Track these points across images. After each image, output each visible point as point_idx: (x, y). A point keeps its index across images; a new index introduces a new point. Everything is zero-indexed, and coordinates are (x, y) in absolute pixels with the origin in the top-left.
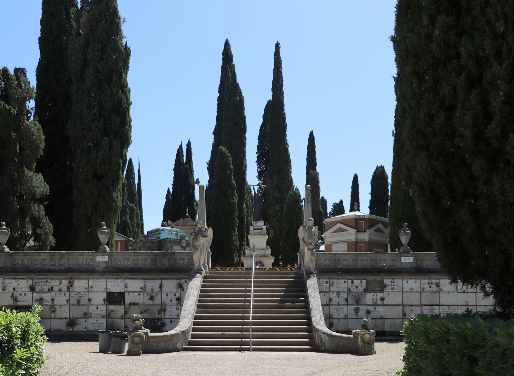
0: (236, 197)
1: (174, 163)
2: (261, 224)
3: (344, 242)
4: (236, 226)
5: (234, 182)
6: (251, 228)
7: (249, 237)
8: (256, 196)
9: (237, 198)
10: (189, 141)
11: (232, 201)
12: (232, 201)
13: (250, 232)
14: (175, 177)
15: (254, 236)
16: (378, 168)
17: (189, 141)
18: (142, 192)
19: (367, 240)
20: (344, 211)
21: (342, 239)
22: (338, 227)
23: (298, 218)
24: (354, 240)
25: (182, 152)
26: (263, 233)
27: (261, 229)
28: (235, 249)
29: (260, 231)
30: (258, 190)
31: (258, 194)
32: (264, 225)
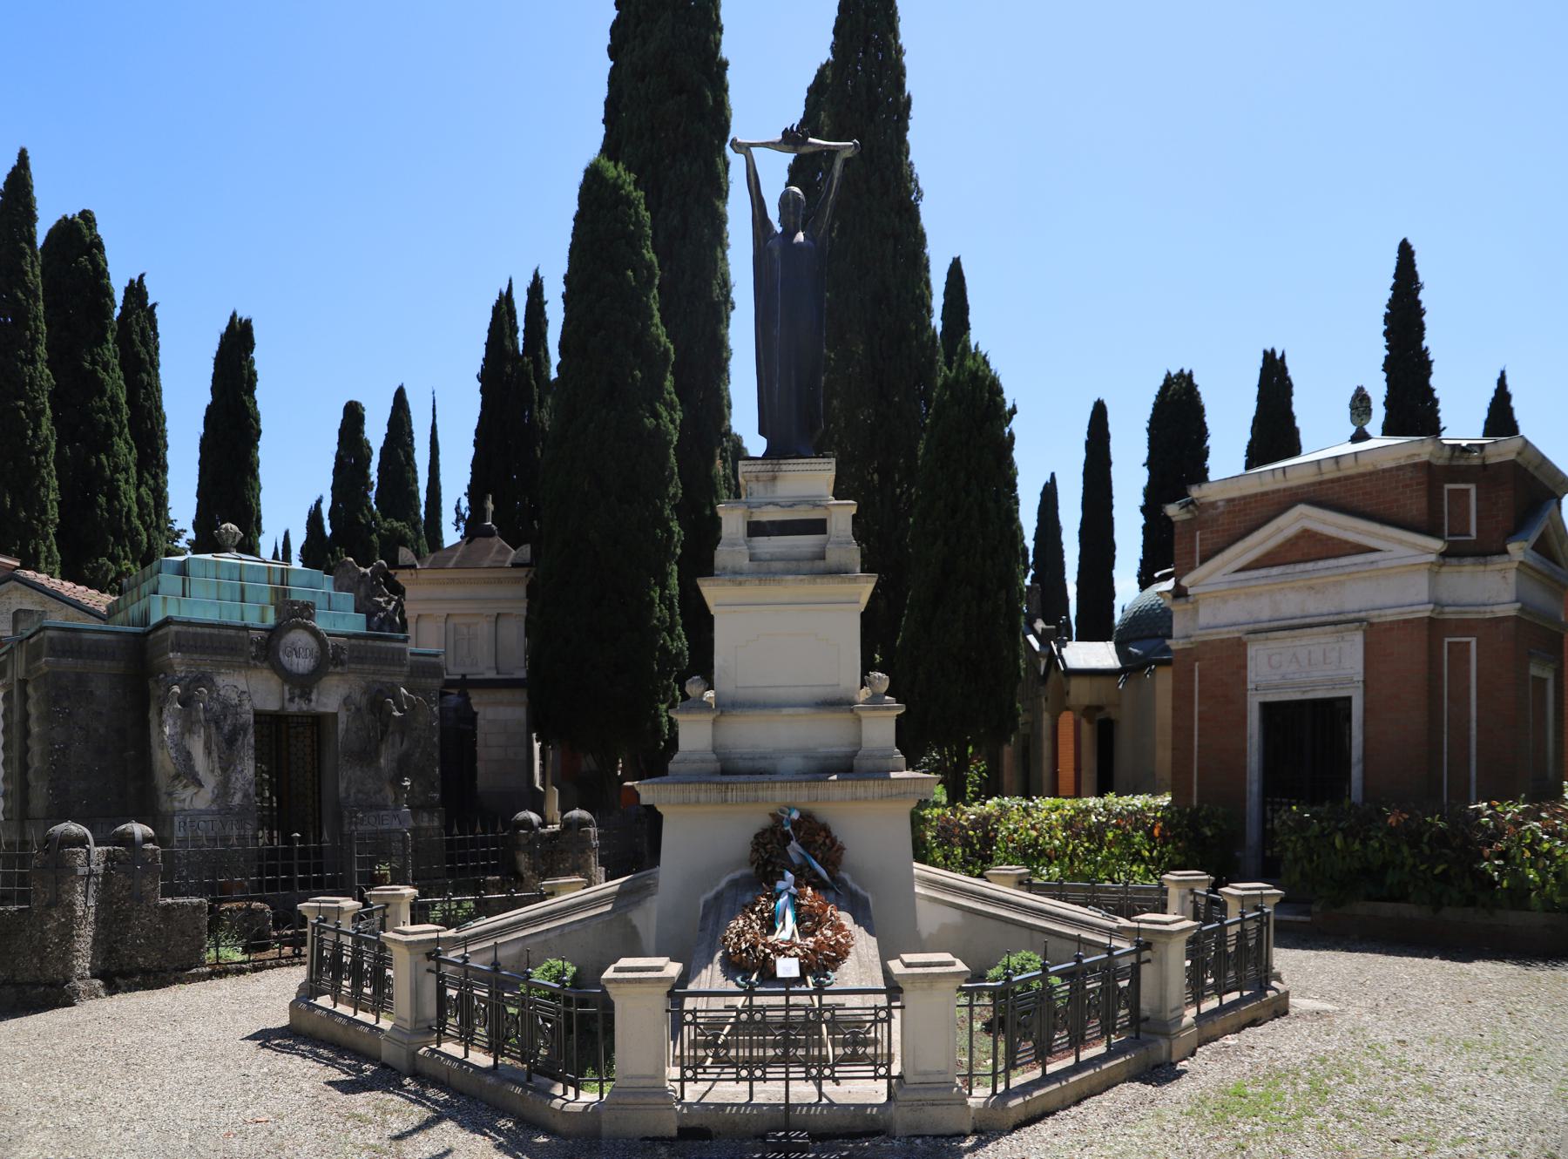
0: (670, 407)
1: (483, 353)
3: (1337, 623)
5: (661, 332)
6: (732, 520)
7: (712, 592)
8: (776, 248)
9: (678, 416)
10: (536, 276)
11: (650, 422)
12: (650, 422)
13: (722, 556)
14: (485, 405)
15: (752, 591)
16: (1168, 380)
17: (536, 276)
18: (443, 491)
19: (1510, 610)
20: (1294, 433)
21: (1316, 605)
22: (1290, 532)
24: (1425, 612)
25: (512, 313)
26: (833, 557)
27: (818, 527)
29: (806, 542)
30: (786, 201)
31: (789, 233)
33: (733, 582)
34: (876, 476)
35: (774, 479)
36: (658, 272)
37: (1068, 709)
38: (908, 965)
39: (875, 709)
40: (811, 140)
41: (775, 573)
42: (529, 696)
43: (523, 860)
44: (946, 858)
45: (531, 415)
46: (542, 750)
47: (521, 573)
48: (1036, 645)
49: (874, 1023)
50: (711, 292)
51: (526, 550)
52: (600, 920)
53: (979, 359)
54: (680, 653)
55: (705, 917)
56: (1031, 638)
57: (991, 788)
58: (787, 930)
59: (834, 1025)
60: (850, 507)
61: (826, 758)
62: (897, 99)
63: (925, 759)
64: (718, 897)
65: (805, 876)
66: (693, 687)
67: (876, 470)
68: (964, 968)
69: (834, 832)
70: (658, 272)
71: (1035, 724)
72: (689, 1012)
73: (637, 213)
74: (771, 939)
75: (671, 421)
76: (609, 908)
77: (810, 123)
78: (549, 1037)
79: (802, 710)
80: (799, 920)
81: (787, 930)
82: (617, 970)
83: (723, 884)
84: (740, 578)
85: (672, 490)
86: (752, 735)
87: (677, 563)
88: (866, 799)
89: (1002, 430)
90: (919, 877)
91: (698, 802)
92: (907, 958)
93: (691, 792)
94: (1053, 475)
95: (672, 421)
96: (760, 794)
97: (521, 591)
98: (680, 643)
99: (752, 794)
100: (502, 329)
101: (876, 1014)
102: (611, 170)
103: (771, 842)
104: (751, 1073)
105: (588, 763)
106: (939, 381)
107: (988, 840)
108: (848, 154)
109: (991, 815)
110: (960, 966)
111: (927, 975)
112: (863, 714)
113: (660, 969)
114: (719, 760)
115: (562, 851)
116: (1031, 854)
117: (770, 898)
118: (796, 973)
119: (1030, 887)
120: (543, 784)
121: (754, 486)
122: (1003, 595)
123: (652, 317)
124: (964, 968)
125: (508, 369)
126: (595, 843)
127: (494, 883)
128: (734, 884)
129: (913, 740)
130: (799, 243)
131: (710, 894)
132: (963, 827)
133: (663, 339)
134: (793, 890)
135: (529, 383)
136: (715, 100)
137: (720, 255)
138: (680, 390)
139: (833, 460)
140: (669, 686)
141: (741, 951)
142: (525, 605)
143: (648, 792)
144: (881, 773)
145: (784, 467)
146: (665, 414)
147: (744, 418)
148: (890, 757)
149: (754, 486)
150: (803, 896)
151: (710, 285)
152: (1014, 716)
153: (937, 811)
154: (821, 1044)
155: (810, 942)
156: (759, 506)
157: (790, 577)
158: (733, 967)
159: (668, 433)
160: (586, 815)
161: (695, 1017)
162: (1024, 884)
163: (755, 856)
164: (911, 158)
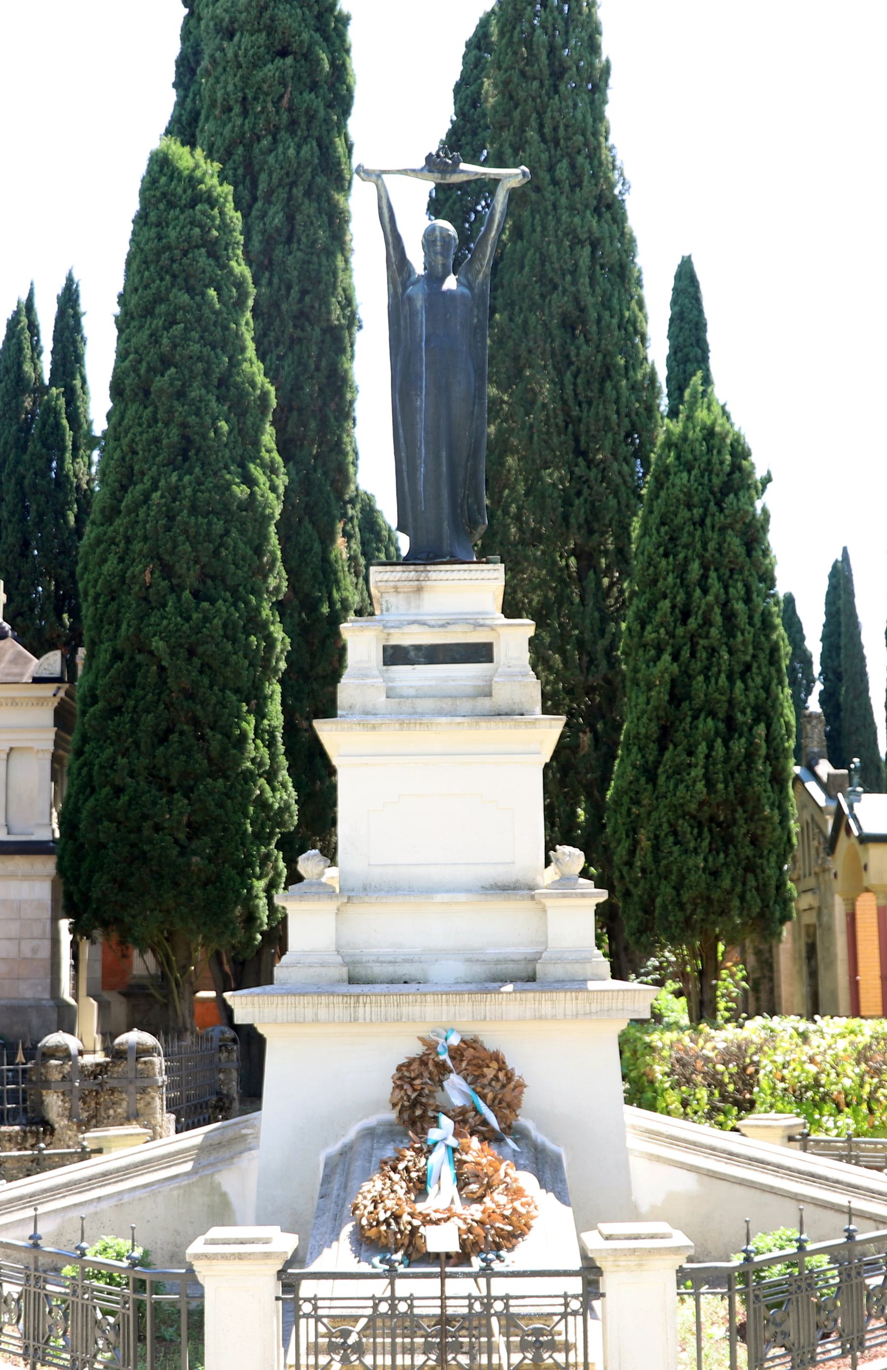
0: (272, 470)
2: (470, 594)
4: (267, 669)
6: (360, 642)
8: (418, 293)
9: (282, 481)
10: (70, 280)
11: (241, 491)
12: (241, 491)
13: (347, 690)
15: (389, 738)
17: (70, 280)
23: (739, 606)
25: (33, 328)
27: (480, 653)
28: (261, 838)
30: (430, 240)
31: (434, 278)
32: (511, 609)
33: (364, 725)
34: (573, 561)
35: (419, 590)
36: (252, 290)
37: (867, 890)
38: (608, 1238)
39: (565, 896)
40: (463, 166)
41: (422, 714)
42: (60, 867)
43: (54, 1104)
44: (685, 1103)
45: (61, 466)
46: (74, 945)
47: (48, 690)
48: (820, 797)
49: (564, 1316)
50: (329, 312)
51: (53, 662)
52: (174, 1184)
53: (716, 409)
54: (286, 808)
55: (327, 1179)
56: (812, 787)
57: (762, 999)
58: (443, 1194)
59: (510, 1321)
60: (526, 628)
61: (498, 962)
62: (591, 65)
63: (653, 962)
64: (346, 1152)
65: (466, 1122)
66: (309, 863)
67: (573, 553)
68: (687, 1242)
69: (510, 1065)
70: (252, 290)
71: (822, 910)
72: (306, 1300)
73: (222, 213)
74: (420, 1207)
75: (271, 489)
76: (188, 1167)
77: (462, 139)
78: (111, 1336)
79: (462, 897)
80: (462, 1182)
81: (443, 1194)
82: (213, 1242)
83: (351, 1134)
84: (372, 720)
85: (272, 582)
86: (388, 931)
87: (281, 681)
88: (554, 1018)
89: (752, 504)
90: (634, 1127)
91: (316, 1021)
92: (608, 1228)
93: (306, 1006)
94: (845, 550)
95: (273, 489)
96: (405, 1009)
97: (47, 716)
98: (284, 795)
99: (392, 1011)
100: (20, 349)
101: (566, 1305)
102: (186, 159)
103: (420, 1076)
104: (393, 1307)
105: (143, 964)
106: (661, 438)
107: (747, 1079)
108: (514, 183)
109: (749, 1042)
110: (680, 1239)
111: (634, 1251)
112: (548, 902)
113: (267, 1241)
114: (346, 964)
115: (112, 1091)
116: (811, 1098)
117: (419, 1151)
118: (454, 1247)
119: (803, 1141)
120: (76, 996)
121: (392, 599)
122: (761, 729)
123: (243, 349)
124: (687, 1242)
125: (28, 403)
126: (162, 1079)
127: (10, 1138)
128: (369, 1133)
129: (624, 941)
130: (450, 291)
131: (334, 1148)
132: (707, 1059)
133: (260, 379)
134: (453, 1142)
135: (58, 425)
136: (332, 64)
137: (340, 263)
138: (284, 447)
139: (501, 567)
140: (268, 856)
141: (379, 1223)
142: (52, 736)
143: (245, 1006)
144: (574, 984)
145: (433, 575)
146: (262, 479)
147: (375, 471)
148: (587, 960)
149: (392, 599)
150: (465, 1150)
151: (328, 304)
152: (785, 901)
153: (670, 1036)
154: (490, 1349)
155: (476, 1211)
156: (400, 625)
157: (443, 720)
158: (367, 1242)
159: (267, 505)
160: (147, 1039)
161: (315, 1308)
162: (801, 1140)
163: (399, 1094)
164: (612, 140)
